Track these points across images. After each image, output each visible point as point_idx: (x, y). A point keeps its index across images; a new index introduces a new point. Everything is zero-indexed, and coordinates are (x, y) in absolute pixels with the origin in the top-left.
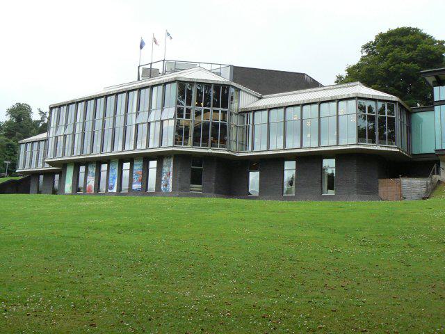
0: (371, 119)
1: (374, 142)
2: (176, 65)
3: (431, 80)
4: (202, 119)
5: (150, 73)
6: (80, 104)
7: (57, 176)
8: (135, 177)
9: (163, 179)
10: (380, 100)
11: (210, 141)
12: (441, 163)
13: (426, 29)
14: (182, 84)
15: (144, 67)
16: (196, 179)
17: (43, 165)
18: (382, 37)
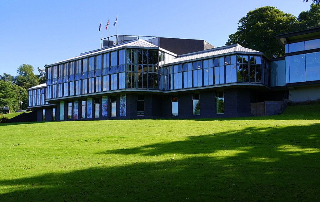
0: (245, 67)
1: (247, 80)
2: (123, 39)
3: (283, 40)
4: (142, 71)
5: (108, 44)
6: (60, 66)
7: (54, 110)
8: (103, 108)
9: (120, 108)
10: (251, 55)
11: (148, 85)
12: (290, 91)
13: (278, 7)
14: (130, 50)
15: (104, 40)
16: (140, 107)
17: (45, 103)
18: (250, 13)
